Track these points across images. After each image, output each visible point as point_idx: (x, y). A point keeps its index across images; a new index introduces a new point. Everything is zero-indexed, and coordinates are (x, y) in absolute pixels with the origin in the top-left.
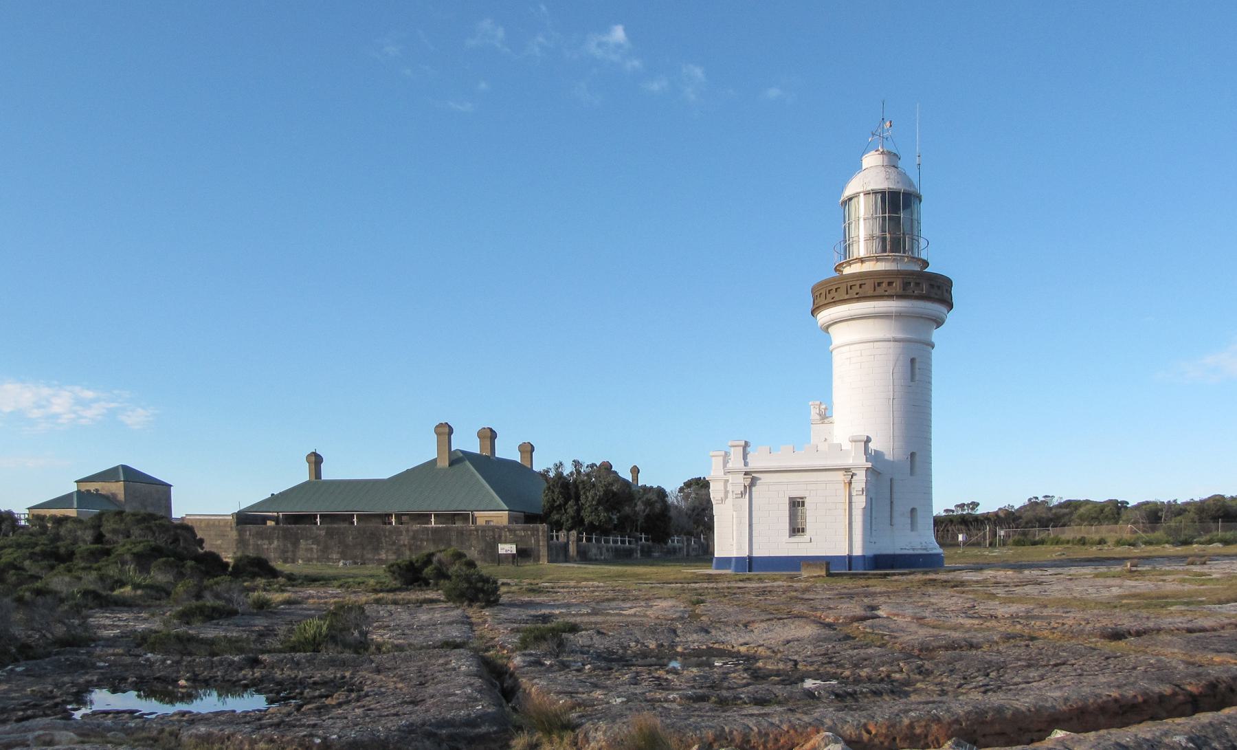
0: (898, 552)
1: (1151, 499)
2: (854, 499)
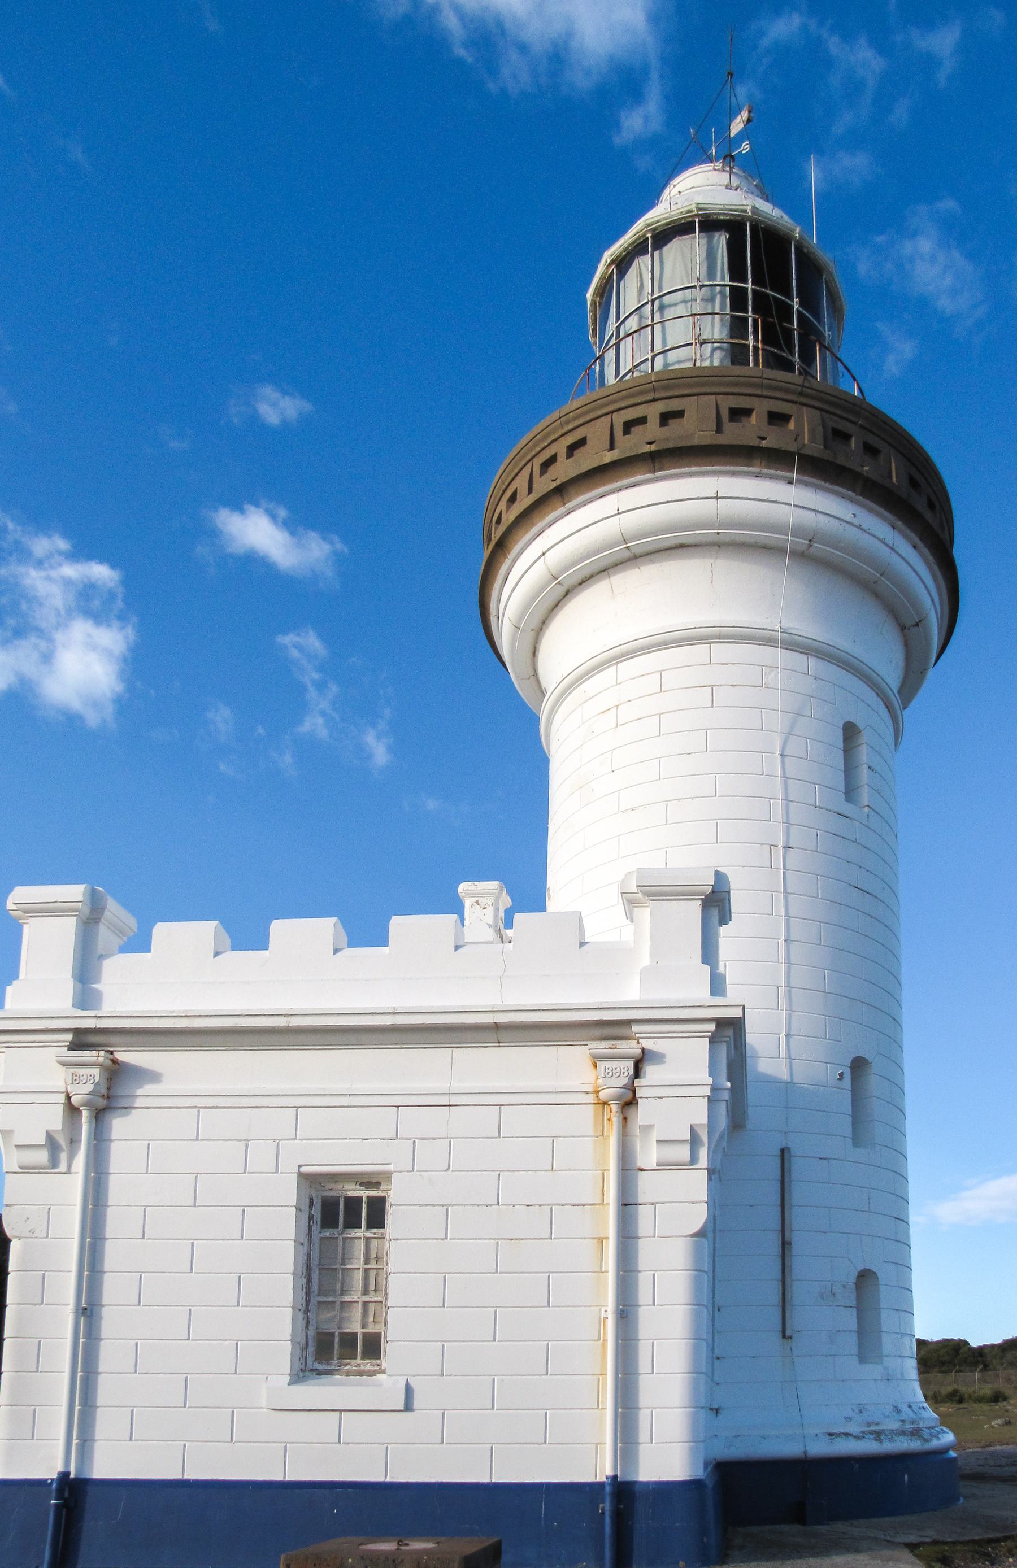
0: (819, 1448)
1: (1009, 1337)
2: (647, 1186)
